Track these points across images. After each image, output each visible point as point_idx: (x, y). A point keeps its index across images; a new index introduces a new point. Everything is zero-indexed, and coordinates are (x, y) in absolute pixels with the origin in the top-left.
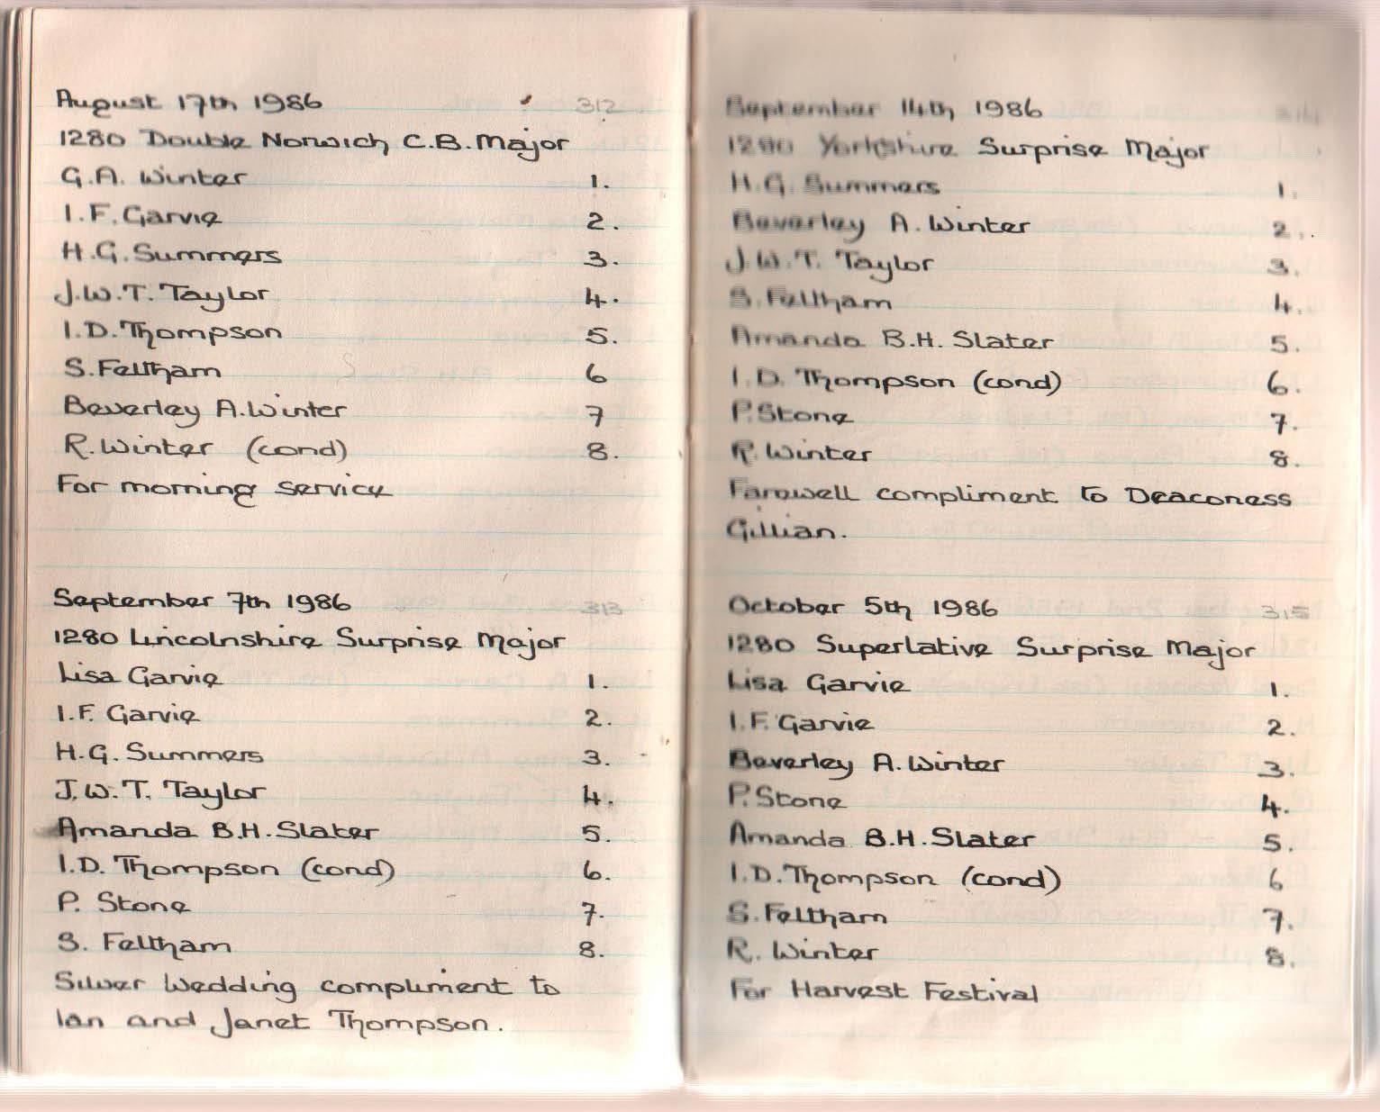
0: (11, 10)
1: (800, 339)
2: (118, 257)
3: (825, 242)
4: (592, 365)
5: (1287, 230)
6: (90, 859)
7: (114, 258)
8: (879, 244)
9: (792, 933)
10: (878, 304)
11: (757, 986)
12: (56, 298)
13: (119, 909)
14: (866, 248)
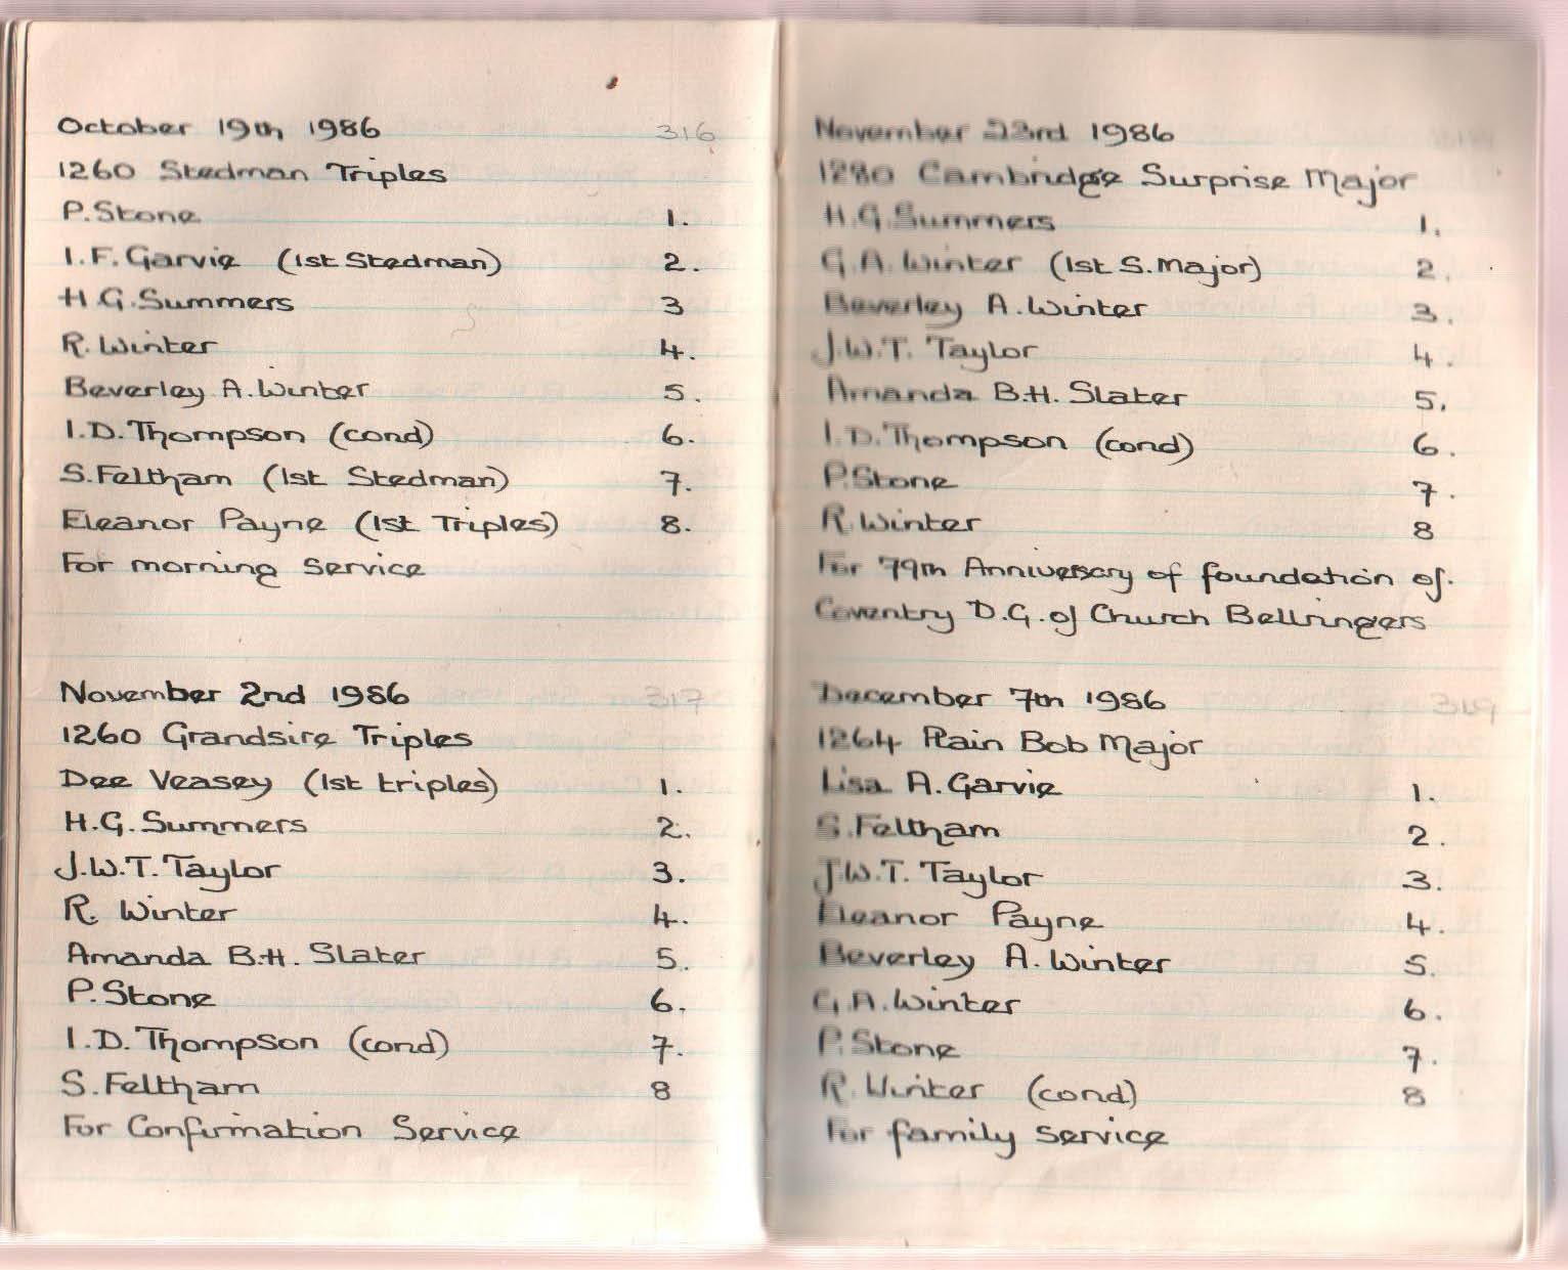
0: (6, 20)
1: (904, 394)
2: (124, 304)
3: (914, 326)
4: (670, 426)
5: (1434, 272)
6: (103, 425)
7: (120, 305)
8: (976, 331)
9: (878, 502)
10: (914, 698)
11: (848, 562)
12: (57, 872)
13: (129, 1002)
14: (961, 335)
